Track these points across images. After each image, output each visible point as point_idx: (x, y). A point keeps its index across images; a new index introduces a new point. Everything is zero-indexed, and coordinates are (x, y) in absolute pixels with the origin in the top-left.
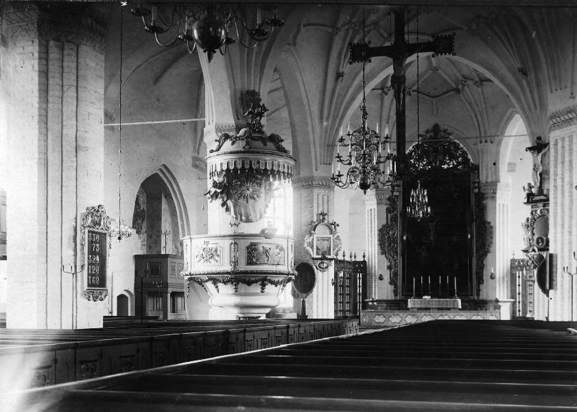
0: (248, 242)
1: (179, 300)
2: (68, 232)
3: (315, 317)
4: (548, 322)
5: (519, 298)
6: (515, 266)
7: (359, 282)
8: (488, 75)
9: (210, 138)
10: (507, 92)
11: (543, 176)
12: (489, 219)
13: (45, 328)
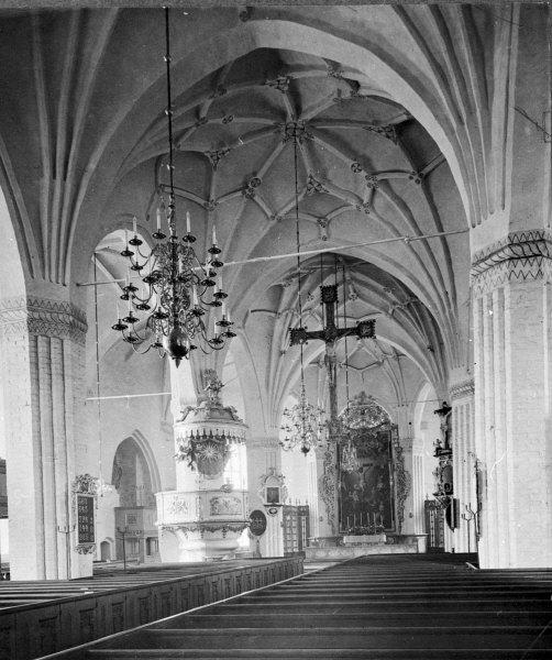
0: (210, 496)
1: (153, 543)
2: (60, 493)
3: (267, 556)
4: (454, 554)
5: (433, 532)
6: (428, 505)
7: (304, 523)
8: (403, 351)
9: (176, 410)
10: (419, 365)
11: (447, 434)
12: (406, 468)
13: (41, 578)
